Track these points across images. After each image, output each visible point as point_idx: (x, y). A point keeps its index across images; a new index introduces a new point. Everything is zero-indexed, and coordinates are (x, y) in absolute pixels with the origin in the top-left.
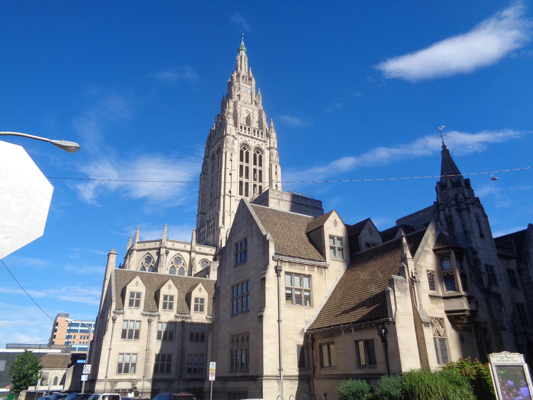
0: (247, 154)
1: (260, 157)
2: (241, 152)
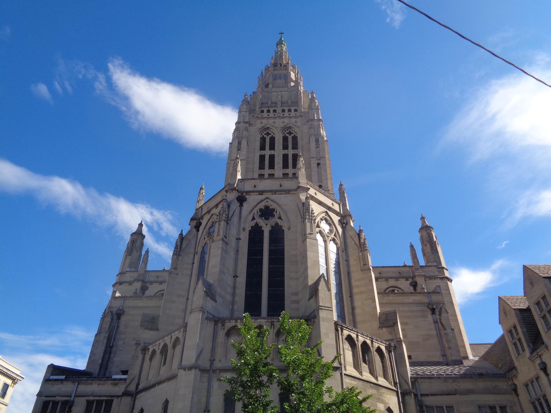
0: (272, 140)
1: (295, 139)
2: (263, 140)
